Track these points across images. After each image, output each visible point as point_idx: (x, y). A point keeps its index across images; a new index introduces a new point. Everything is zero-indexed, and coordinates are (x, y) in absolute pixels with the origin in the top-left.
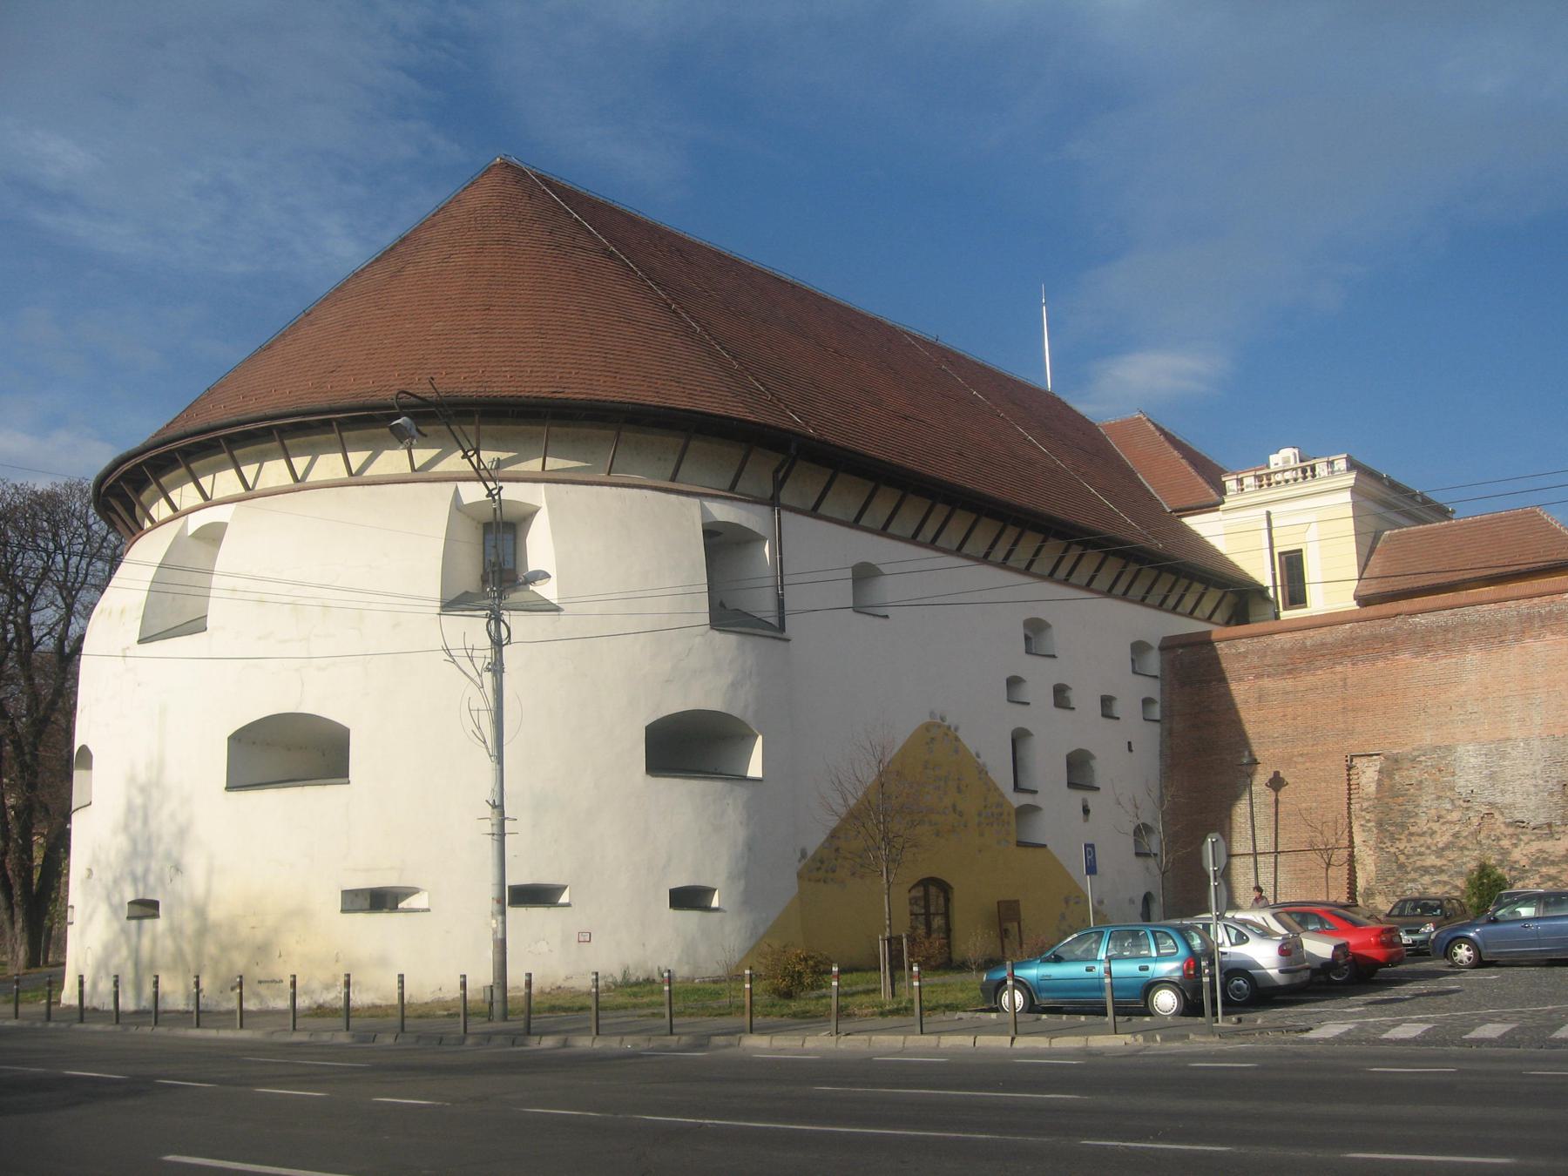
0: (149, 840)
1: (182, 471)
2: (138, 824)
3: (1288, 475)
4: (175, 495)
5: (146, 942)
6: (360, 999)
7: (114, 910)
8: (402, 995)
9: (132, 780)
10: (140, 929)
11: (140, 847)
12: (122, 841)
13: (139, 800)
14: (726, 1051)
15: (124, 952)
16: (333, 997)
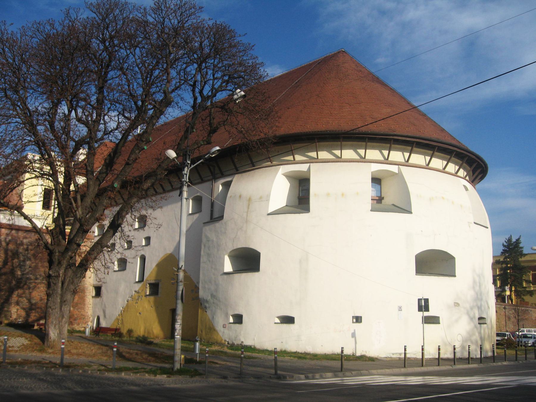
0: (481, 294)
2: (477, 288)
5: (482, 331)
6: (345, 352)
7: (472, 319)
10: (480, 327)
11: (479, 296)
13: (477, 279)
14: (157, 348)
15: (477, 334)
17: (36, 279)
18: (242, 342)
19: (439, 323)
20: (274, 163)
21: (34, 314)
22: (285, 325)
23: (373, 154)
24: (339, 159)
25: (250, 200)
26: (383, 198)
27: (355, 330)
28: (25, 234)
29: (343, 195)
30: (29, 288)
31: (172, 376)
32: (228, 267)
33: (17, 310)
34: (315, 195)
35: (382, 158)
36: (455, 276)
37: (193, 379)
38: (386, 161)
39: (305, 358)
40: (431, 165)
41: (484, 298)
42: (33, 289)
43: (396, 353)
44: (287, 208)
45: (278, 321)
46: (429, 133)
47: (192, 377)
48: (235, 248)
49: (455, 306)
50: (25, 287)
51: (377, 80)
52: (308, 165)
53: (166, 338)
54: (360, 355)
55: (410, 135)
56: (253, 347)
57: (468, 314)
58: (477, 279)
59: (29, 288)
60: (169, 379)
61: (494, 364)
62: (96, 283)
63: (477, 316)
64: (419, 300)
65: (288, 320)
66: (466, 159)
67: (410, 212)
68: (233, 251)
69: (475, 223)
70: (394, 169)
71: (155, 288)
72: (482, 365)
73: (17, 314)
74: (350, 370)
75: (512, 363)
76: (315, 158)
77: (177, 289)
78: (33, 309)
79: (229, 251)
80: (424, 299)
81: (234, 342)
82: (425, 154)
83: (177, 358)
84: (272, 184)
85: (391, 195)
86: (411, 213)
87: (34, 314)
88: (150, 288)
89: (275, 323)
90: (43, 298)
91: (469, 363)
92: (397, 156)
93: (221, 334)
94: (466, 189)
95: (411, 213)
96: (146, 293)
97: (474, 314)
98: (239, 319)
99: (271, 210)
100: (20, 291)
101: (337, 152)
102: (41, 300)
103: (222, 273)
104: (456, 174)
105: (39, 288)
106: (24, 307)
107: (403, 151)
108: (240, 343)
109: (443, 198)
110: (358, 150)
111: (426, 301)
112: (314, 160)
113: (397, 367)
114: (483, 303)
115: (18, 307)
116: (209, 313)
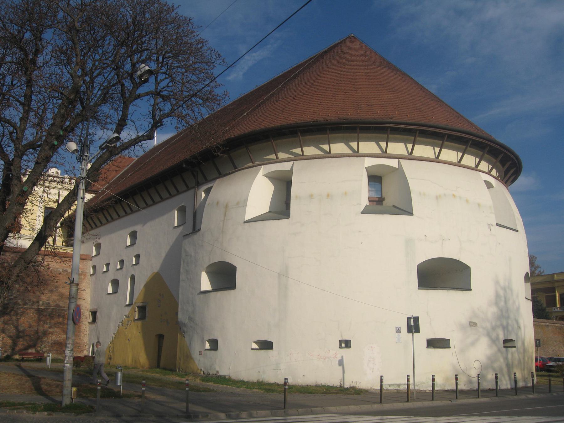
0: (507, 310)
1: (481, 153)
2: (502, 304)
3: (57, 179)
4: (483, 163)
5: (510, 356)
7: (494, 341)
8: (381, 386)
9: (497, 283)
10: (507, 351)
12: (494, 309)
13: (501, 293)
15: (502, 360)
16: (451, 386)
17: (25, 304)
18: (217, 372)
19: (450, 347)
20: (256, 163)
21: (22, 343)
22: (262, 351)
23: (368, 147)
24: (328, 155)
25: (227, 207)
26: (384, 199)
27: (342, 357)
28: (13, 255)
29: (328, 195)
30: (17, 314)
31: (54, 414)
32: (205, 284)
33: (3, 338)
34: (297, 197)
35: (379, 152)
36: (470, 290)
37: (79, 417)
38: (384, 155)
39: (273, 391)
40: (463, 162)
41: (512, 316)
42: (21, 316)
43: (394, 385)
44: (270, 214)
45: (255, 346)
46: (439, 119)
47: (78, 414)
48: (211, 263)
49: (471, 326)
50: (13, 312)
51: (389, 66)
52: (291, 163)
53: (151, 367)
54: (348, 386)
55: (410, 122)
56: (227, 377)
57: (488, 335)
58: (501, 293)
59: (17, 314)
60: (49, 417)
61: (516, 397)
62: (94, 307)
63: (502, 337)
64: (409, 319)
65: (266, 345)
66: (487, 149)
67: (411, 214)
68: (210, 265)
69: (498, 225)
70: (394, 163)
71: (142, 309)
72: (496, 399)
73: (3, 343)
74: (298, 406)
75: (542, 395)
76: (300, 155)
77: (162, 314)
78: (21, 337)
79: (206, 266)
80: (414, 318)
81: (209, 371)
82: (434, 145)
83: (66, 391)
84: (256, 190)
85: (391, 196)
86: (412, 214)
87: (22, 343)
88: (139, 312)
89: (252, 349)
90: (32, 324)
91: (479, 397)
92: (397, 147)
93: (197, 362)
94: (489, 185)
95: (412, 214)
96: (135, 317)
97: (498, 335)
98: (214, 344)
99: (247, 218)
100: (7, 318)
101: (326, 147)
102: (30, 326)
103: (198, 292)
104: (476, 168)
105: (28, 314)
106: (11, 334)
107: (405, 142)
108: (215, 372)
109: (454, 196)
110: (351, 143)
111: (416, 319)
112: (298, 158)
113: (401, 402)
114: (510, 322)
115: (4, 335)
116: (187, 339)
